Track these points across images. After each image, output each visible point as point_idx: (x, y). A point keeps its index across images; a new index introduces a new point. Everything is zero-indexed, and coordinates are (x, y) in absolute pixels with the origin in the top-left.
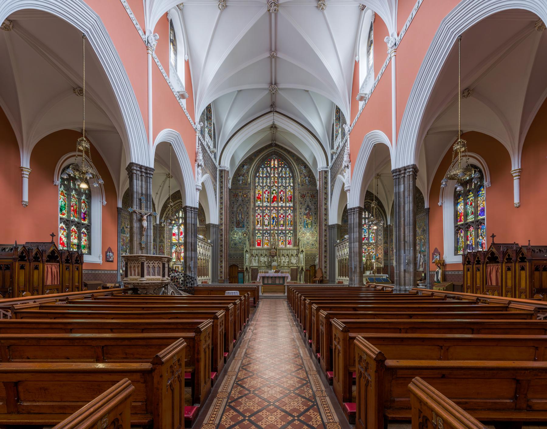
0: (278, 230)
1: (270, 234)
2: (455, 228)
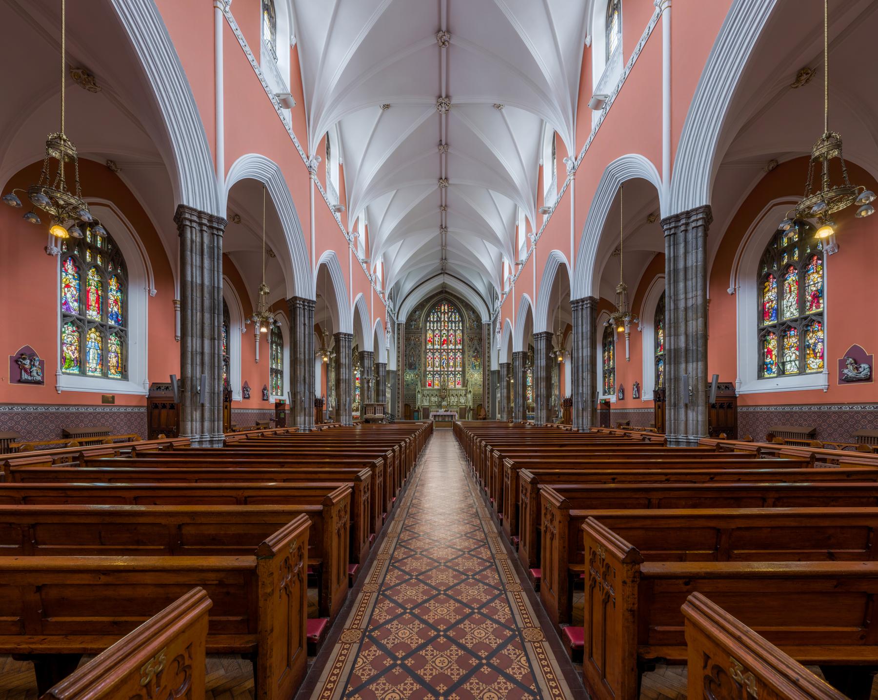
0: (448, 371)
1: (440, 375)
2: (655, 359)
